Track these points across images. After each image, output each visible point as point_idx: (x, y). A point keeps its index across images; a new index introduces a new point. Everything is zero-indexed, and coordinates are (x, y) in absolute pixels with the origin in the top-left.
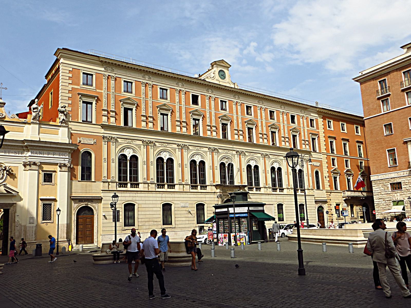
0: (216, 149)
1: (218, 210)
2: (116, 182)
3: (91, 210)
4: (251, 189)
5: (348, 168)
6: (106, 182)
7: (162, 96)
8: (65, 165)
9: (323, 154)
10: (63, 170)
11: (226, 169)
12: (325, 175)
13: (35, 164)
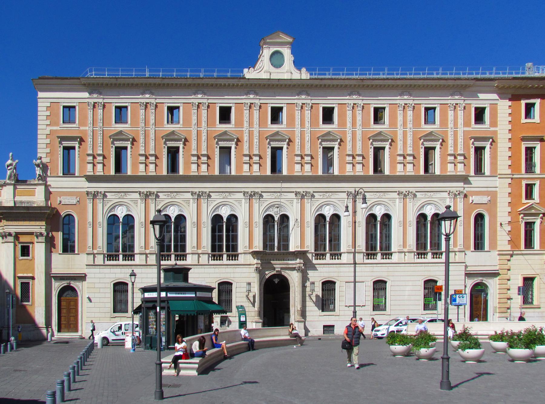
0: (257, 193)
1: (147, 295)
2: (414, 252)
3: (73, 290)
4: (320, 256)
6: (91, 254)
8: (41, 234)
9: (503, 177)
10: (40, 241)
11: (275, 226)
12: (499, 220)
13: (10, 234)
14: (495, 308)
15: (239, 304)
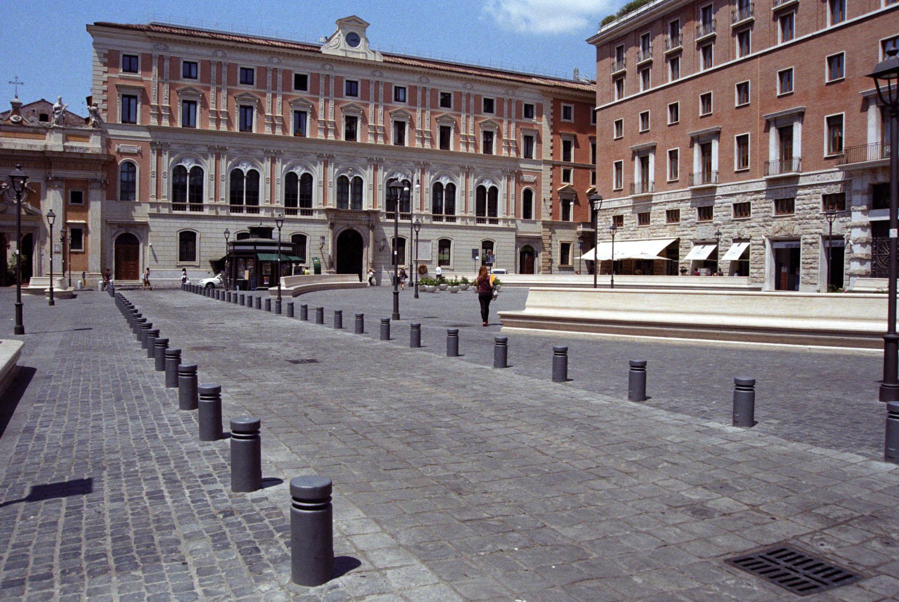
5: (567, 184)
7: (244, 79)
14: (539, 268)
15: (313, 256)
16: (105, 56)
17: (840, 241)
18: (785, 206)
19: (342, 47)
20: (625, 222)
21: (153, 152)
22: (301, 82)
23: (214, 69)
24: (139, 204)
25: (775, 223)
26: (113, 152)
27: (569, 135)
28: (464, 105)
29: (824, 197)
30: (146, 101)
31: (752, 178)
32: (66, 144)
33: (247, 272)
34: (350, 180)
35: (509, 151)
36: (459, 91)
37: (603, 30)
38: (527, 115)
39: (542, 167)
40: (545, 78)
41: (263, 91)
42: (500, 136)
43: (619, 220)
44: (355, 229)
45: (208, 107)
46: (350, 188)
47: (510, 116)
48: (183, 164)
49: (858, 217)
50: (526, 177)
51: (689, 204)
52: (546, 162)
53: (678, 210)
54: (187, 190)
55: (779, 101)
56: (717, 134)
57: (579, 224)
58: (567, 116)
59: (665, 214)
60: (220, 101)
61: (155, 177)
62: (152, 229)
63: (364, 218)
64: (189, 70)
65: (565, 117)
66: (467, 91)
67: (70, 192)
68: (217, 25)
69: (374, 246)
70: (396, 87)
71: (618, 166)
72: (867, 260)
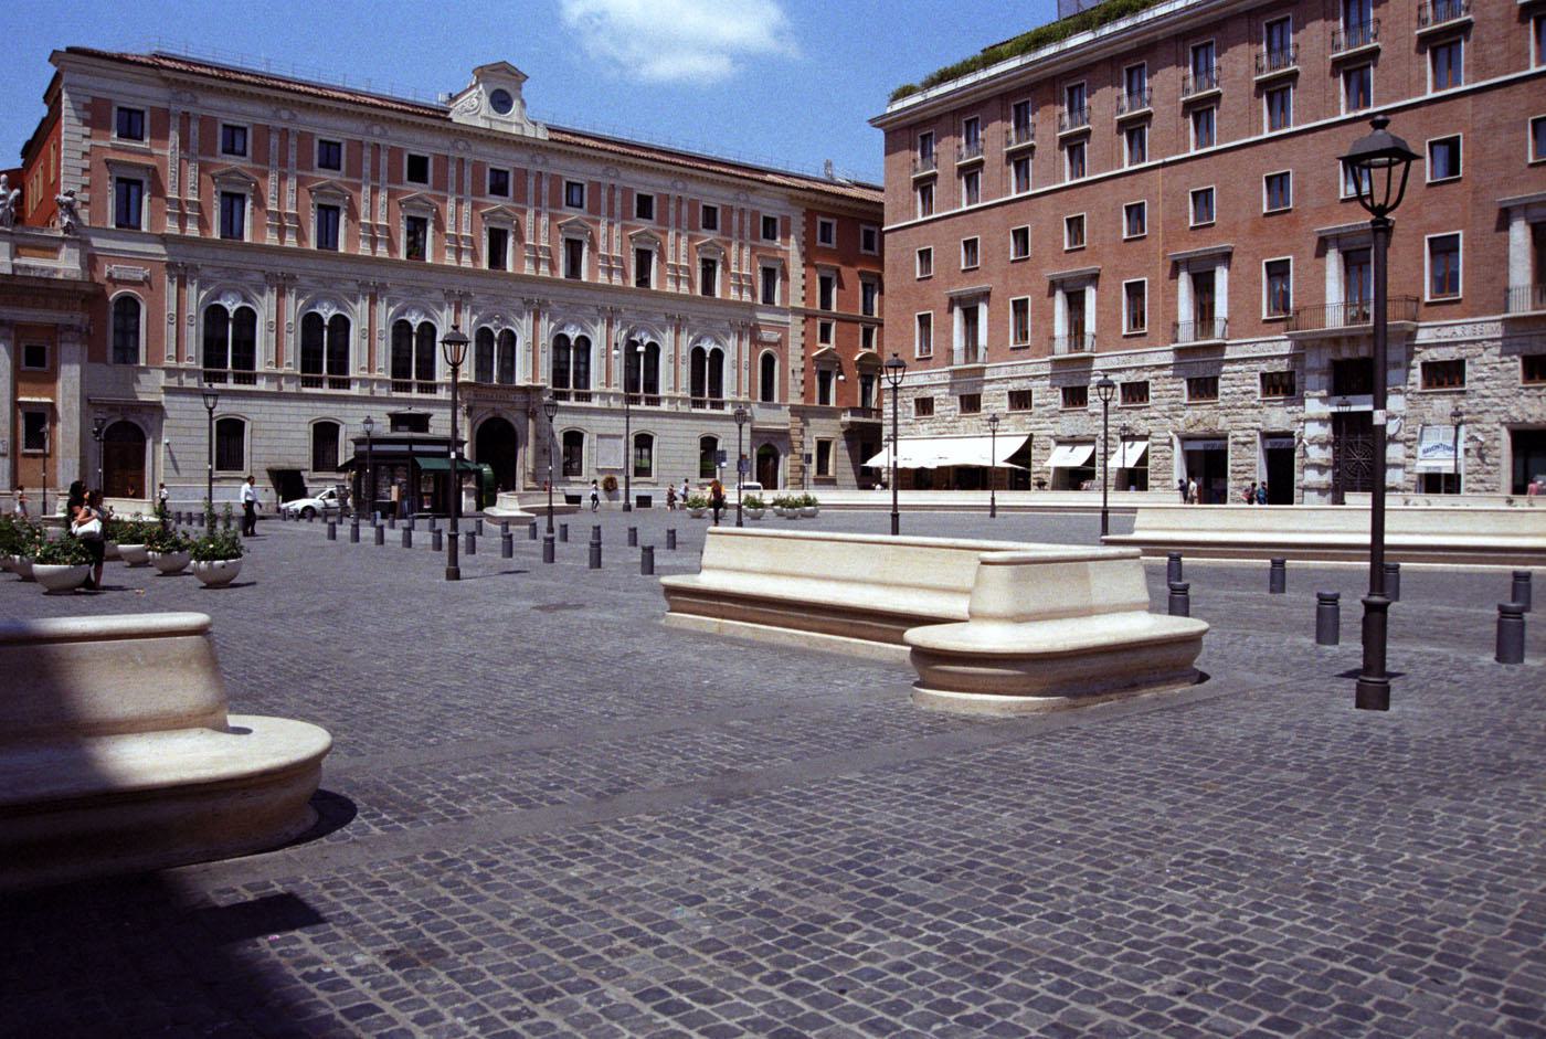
5: (826, 347)
12: (791, 366)
14: (786, 480)
16: (86, 107)
17: (1286, 441)
18: (1204, 388)
19: (483, 112)
20: (936, 408)
21: (171, 281)
22: (418, 169)
23: (274, 140)
24: (145, 370)
25: (1188, 413)
26: (101, 277)
27: (826, 267)
28: (672, 215)
29: (1263, 376)
30: (158, 191)
31: (1151, 345)
32: (16, 261)
33: (395, 489)
34: (496, 335)
35: (741, 291)
36: (358, 138)
37: (889, 110)
38: (766, 236)
39: (790, 318)
40: (787, 176)
41: (441, 194)
42: (520, 238)
43: (925, 406)
44: (505, 416)
45: (265, 205)
46: (495, 348)
47: (741, 236)
48: (222, 302)
49: (1316, 406)
50: (766, 335)
51: (1048, 382)
52: (796, 311)
53: (1030, 392)
54: (227, 345)
55: (1192, 235)
56: (1094, 278)
57: (844, 410)
58: (826, 238)
59: (1006, 398)
60: (284, 195)
61: (174, 324)
62: (170, 414)
63: (519, 399)
64: (233, 139)
65: (823, 240)
66: (458, 155)
67: (23, 346)
68: (268, 62)
69: (536, 446)
70: (568, 183)
71: (925, 321)
72: (1327, 467)
